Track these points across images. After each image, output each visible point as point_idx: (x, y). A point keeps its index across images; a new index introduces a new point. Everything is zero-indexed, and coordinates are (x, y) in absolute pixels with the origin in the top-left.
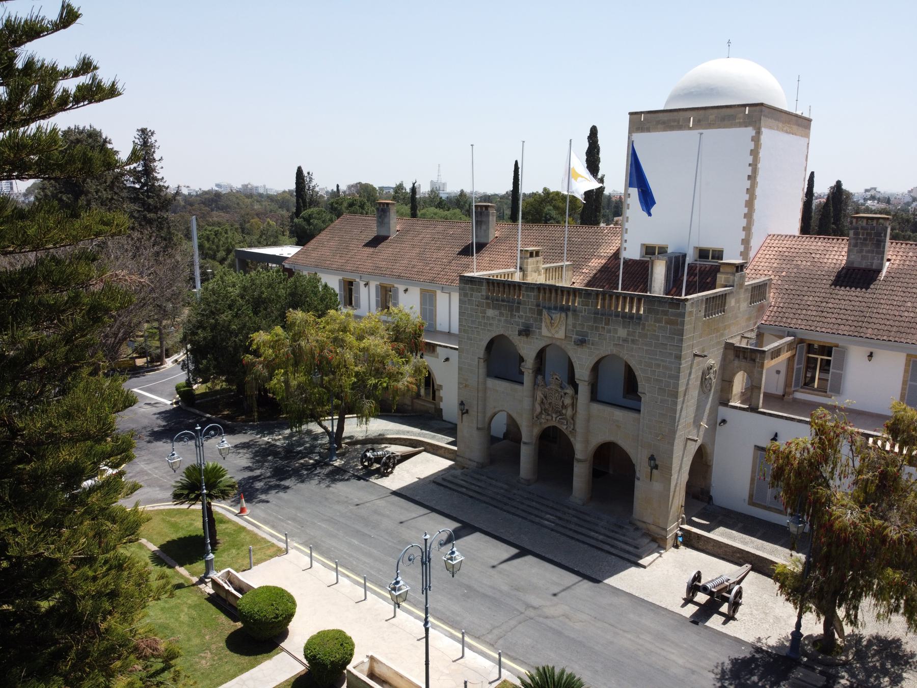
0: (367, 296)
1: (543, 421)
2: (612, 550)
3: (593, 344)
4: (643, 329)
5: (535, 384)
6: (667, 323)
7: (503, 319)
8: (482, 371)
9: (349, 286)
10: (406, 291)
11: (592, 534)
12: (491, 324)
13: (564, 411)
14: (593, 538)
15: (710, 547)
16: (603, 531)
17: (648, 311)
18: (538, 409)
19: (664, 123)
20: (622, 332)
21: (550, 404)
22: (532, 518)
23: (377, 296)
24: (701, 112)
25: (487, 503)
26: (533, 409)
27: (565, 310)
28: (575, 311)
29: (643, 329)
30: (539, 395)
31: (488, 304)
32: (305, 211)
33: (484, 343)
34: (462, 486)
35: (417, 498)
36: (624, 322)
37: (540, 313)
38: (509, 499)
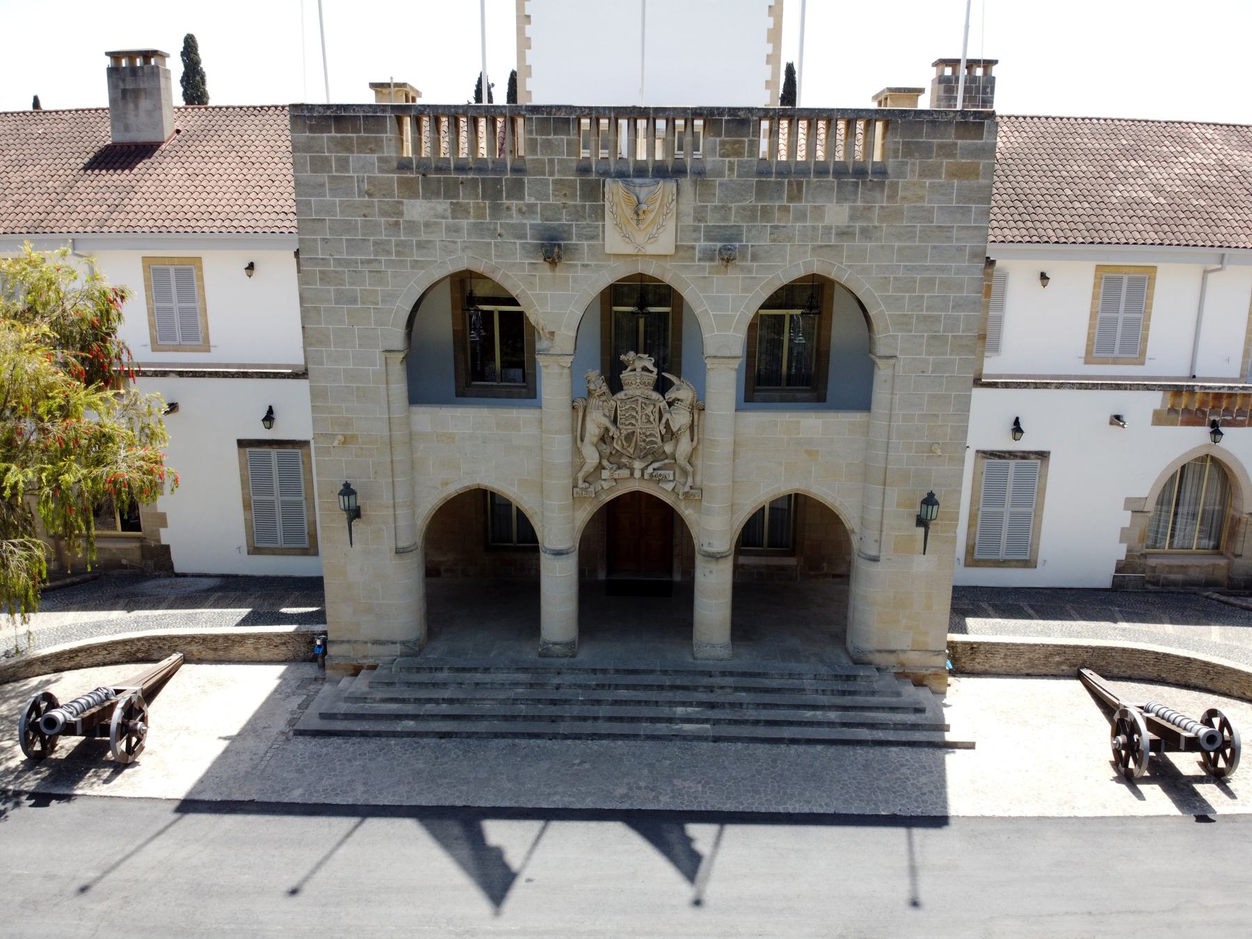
1: (606, 485)
2: (880, 735)
3: (755, 258)
4: (892, 197)
6: (952, 175)
7: (464, 223)
11: (809, 714)
12: (421, 245)
13: (668, 448)
14: (819, 724)
15: (998, 662)
16: (825, 700)
18: (591, 456)
20: (836, 213)
21: (629, 437)
22: (645, 728)
25: (503, 735)
28: (700, 173)
29: (892, 197)
30: (596, 421)
31: (404, 183)
34: (398, 717)
35: (296, 796)
36: (841, 186)
38: (553, 702)
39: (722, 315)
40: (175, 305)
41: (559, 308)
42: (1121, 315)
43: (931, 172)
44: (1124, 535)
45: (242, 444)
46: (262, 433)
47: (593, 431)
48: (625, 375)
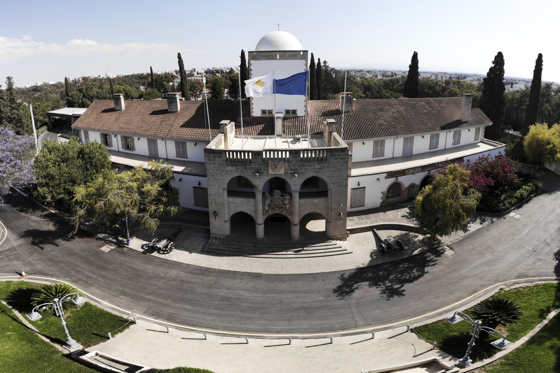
3: (301, 174)
4: (329, 164)
10: (139, 139)
18: (267, 208)
19: (266, 56)
23: (122, 141)
24: (283, 53)
29: (329, 164)
30: (268, 202)
34: (225, 251)
39: (295, 184)
40: (181, 149)
41: (260, 182)
42: (379, 148)
43: (337, 159)
44: (381, 198)
45: (194, 187)
46: (198, 186)
47: (267, 203)
48: (274, 194)
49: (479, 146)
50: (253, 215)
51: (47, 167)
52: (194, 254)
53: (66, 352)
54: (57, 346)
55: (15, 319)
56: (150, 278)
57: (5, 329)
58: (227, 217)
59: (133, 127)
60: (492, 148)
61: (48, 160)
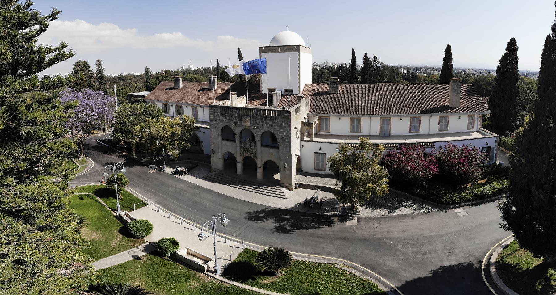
0: (172, 110)
5: (241, 142)
8: (220, 138)
9: (166, 106)
17: (279, 115)
18: (242, 151)
20: (270, 123)
26: (241, 151)
27: (249, 116)
30: (242, 146)
32: (149, 81)
33: (220, 129)
37: (240, 117)
42: (356, 125)
49: (471, 135)
50: (235, 155)
51: (122, 118)
52: (198, 179)
53: (116, 215)
54: (113, 212)
55: (98, 201)
56: (168, 186)
57: (92, 205)
58: (221, 155)
59: (184, 100)
60: (482, 136)
61: (123, 113)
